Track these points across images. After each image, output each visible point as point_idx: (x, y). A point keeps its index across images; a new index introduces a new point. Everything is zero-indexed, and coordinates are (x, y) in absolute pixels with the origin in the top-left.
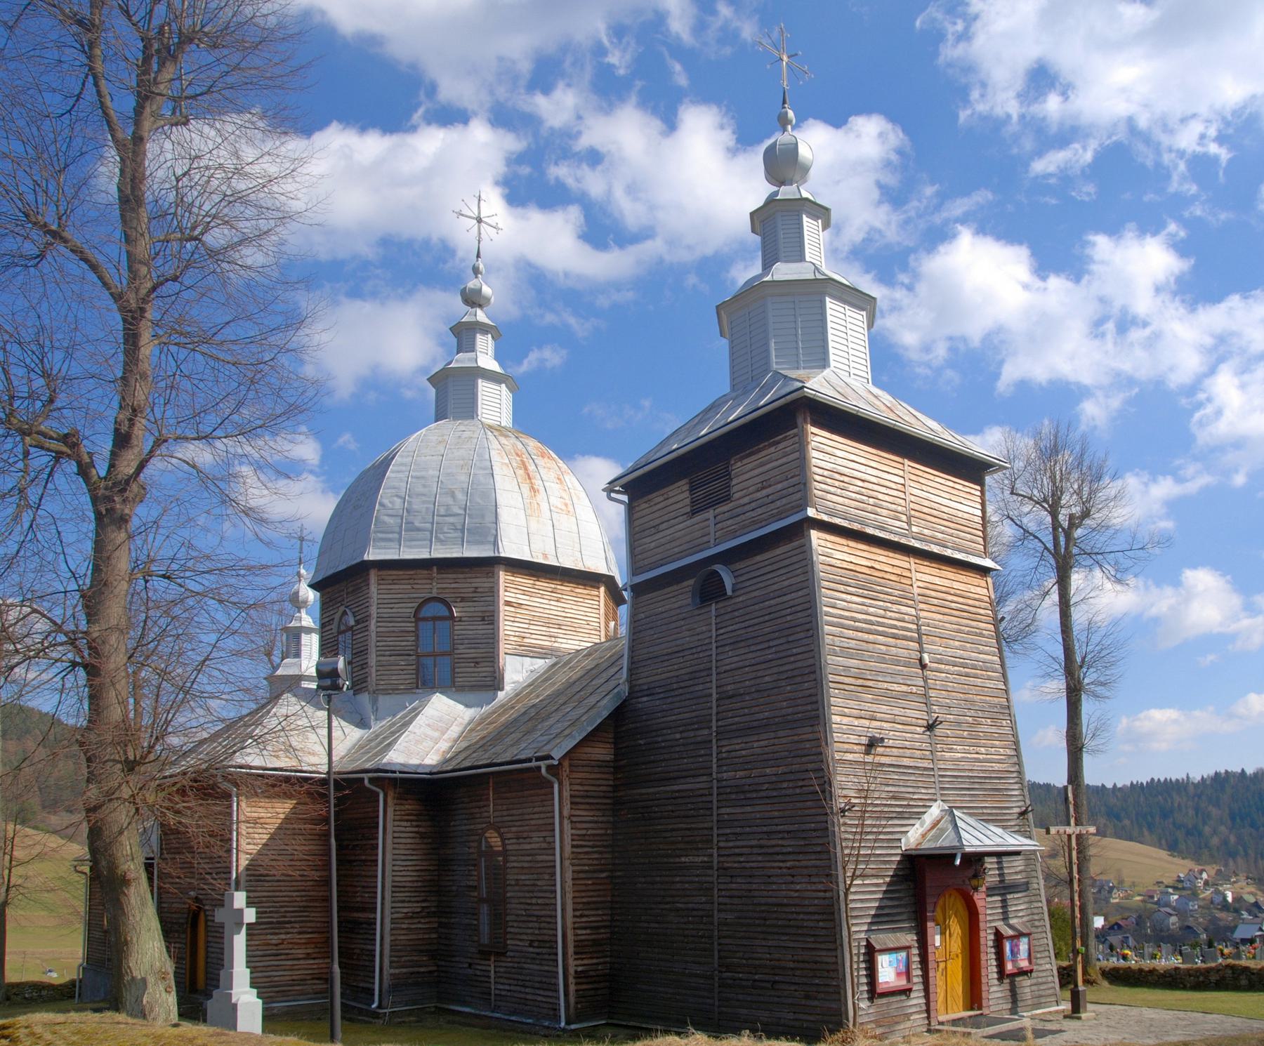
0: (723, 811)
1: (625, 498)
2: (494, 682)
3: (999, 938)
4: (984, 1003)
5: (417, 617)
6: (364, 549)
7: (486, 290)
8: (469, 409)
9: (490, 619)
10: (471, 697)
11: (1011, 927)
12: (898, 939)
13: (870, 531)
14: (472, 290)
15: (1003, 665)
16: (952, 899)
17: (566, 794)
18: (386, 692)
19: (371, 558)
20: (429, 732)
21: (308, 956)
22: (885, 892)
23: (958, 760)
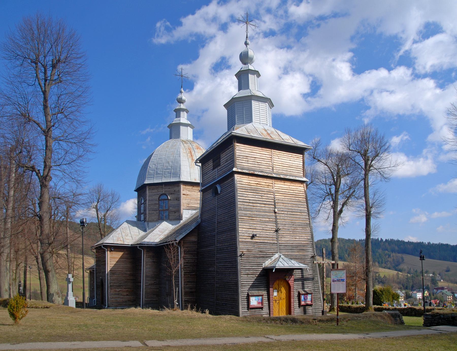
0: (218, 255)
1: (200, 164)
2: (180, 218)
3: (299, 295)
4: (292, 313)
5: (159, 200)
6: (144, 181)
7: (184, 98)
8: (178, 135)
9: (178, 199)
10: (174, 222)
11: (304, 291)
12: (258, 293)
13: (256, 173)
14: (179, 98)
15: (308, 211)
16: (282, 283)
18: (151, 221)
19: (146, 183)
20: (159, 233)
21: (127, 295)
22: (256, 279)
23: (287, 241)
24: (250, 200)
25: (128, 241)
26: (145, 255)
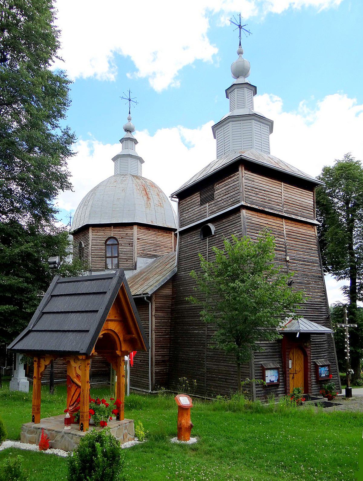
1: (177, 200)
13: (267, 210)
17: (154, 307)
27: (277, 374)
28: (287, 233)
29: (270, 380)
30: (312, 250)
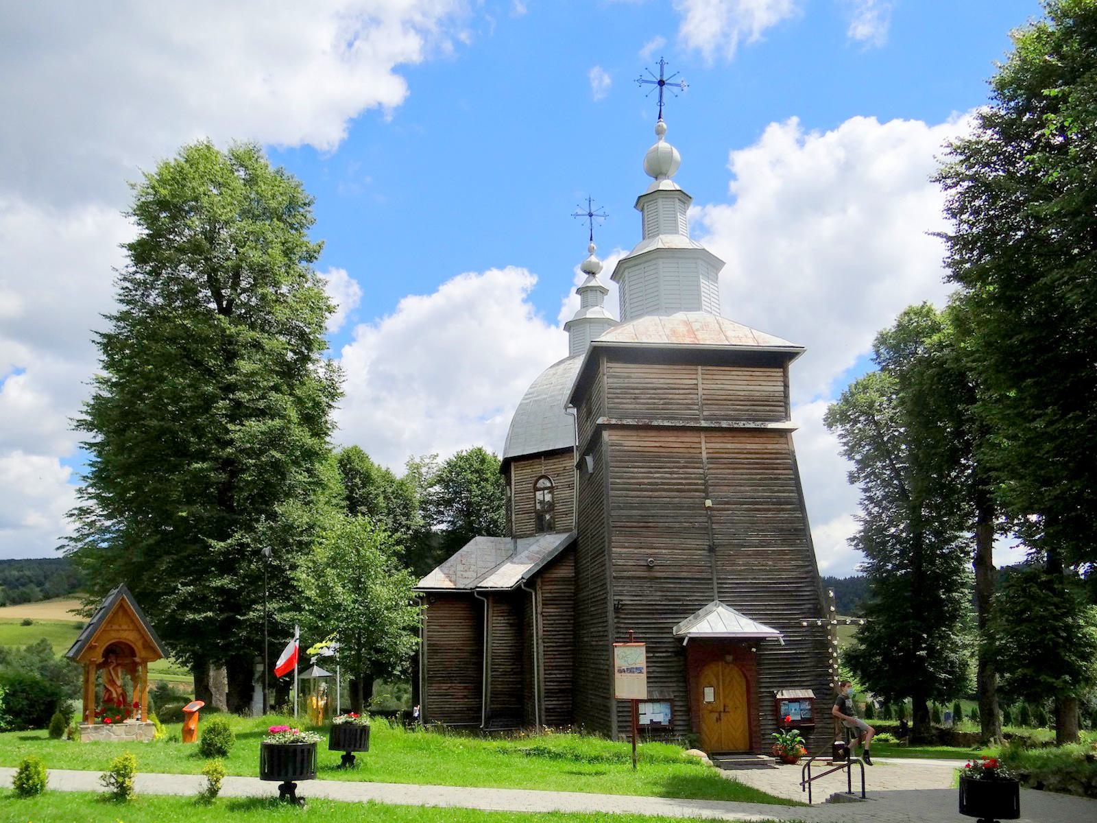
13: (655, 423)
17: (540, 599)
21: (465, 697)
24: (640, 484)
25: (467, 581)
26: (490, 610)
27: (668, 711)
28: (708, 455)
29: (651, 720)
30: (779, 479)
